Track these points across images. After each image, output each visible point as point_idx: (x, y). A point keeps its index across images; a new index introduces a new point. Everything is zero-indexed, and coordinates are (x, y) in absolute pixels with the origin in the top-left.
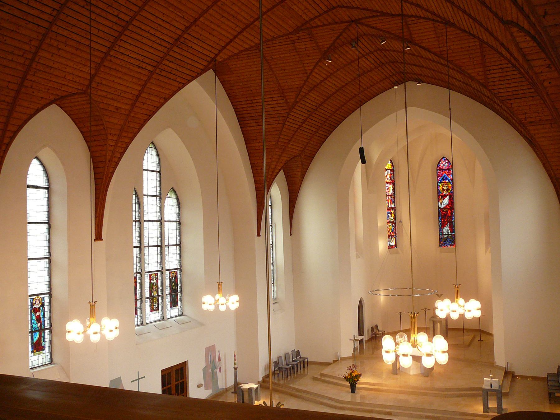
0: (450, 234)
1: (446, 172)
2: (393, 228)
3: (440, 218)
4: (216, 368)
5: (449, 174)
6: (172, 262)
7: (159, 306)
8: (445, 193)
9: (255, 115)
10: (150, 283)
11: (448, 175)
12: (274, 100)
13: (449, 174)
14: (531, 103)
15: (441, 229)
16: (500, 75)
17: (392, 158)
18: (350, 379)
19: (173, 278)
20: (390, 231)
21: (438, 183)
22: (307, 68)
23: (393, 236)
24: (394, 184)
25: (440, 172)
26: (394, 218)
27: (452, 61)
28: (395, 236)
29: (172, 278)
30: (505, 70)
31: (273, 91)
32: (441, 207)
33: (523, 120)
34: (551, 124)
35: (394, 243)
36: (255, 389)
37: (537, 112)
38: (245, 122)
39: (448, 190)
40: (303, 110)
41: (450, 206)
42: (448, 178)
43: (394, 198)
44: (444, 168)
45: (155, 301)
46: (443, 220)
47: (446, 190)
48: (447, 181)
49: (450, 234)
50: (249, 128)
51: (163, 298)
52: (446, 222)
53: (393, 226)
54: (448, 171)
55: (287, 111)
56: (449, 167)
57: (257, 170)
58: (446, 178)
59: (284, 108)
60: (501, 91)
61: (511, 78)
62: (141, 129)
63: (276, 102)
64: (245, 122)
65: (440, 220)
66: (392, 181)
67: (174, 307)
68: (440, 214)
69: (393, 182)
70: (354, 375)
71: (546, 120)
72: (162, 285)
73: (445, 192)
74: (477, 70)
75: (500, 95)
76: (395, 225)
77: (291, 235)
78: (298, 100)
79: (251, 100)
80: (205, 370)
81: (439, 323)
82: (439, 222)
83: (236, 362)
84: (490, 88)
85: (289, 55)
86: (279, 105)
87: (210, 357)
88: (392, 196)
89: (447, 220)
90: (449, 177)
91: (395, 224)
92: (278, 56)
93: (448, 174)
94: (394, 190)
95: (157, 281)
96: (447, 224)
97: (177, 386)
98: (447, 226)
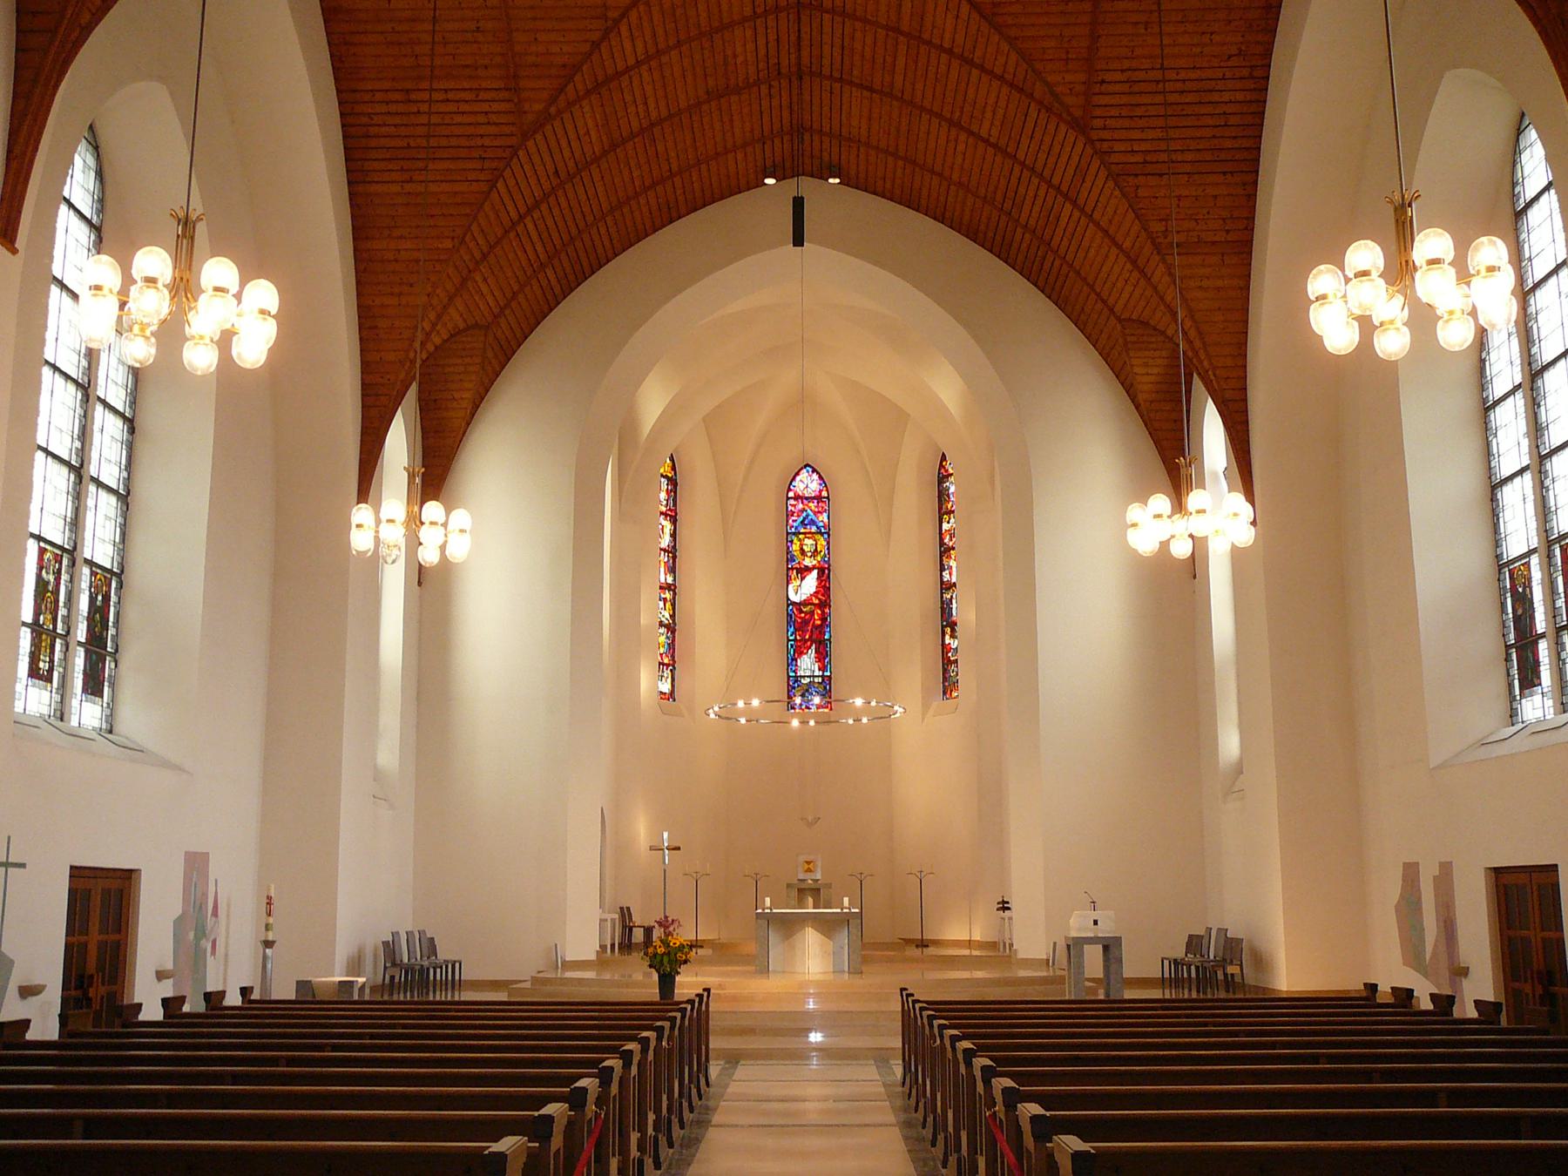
0: (816, 676)
1: (811, 504)
2: (669, 644)
3: (792, 629)
4: (204, 935)
5: (819, 512)
6: (100, 547)
7: (53, 670)
8: (808, 562)
10: (39, 576)
11: (815, 513)
13: (819, 512)
14: (1184, 192)
16: (1125, 100)
19: (100, 598)
20: (662, 652)
21: (788, 533)
24: (674, 521)
25: (795, 503)
26: (670, 616)
28: (671, 668)
29: (97, 595)
30: (1136, 88)
31: (486, 67)
32: (794, 598)
33: (1158, 237)
34: (1223, 255)
37: (1194, 217)
39: (815, 553)
40: (547, 159)
41: (819, 599)
42: (816, 520)
43: (674, 558)
44: (807, 495)
45: (46, 647)
46: (800, 636)
47: (809, 554)
48: (814, 529)
49: (819, 676)
50: (373, 188)
51: (67, 646)
52: (806, 641)
53: (667, 638)
54: (818, 503)
55: (513, 141)
56: (821, 491)
57: (376, 327)
58: (813, 522)
59: (507, 130)
61: (1147, 114)
65: (791, 635)
66: (670, 510)
67: (93, 697)
68: (791, 618)
69: (673, 514)
70: (675, 944)
71: (1214, 243)
72: (69, 601)
73: (807, 560)
76: (674, 637)
77: (420, 583)
78: (553, 110)
80: (179, 923)
82: (789, 640)
83: (271, 920)
84: (1094, 135)
86: (494, 118)
87: (195, 887)
90: (821, 519)
91: (673, 632)
93: (816, 510)
94: (674, 535)
95: (58, 579)
96: (810, 648)
97: (102, 946)
98: (810, 651)
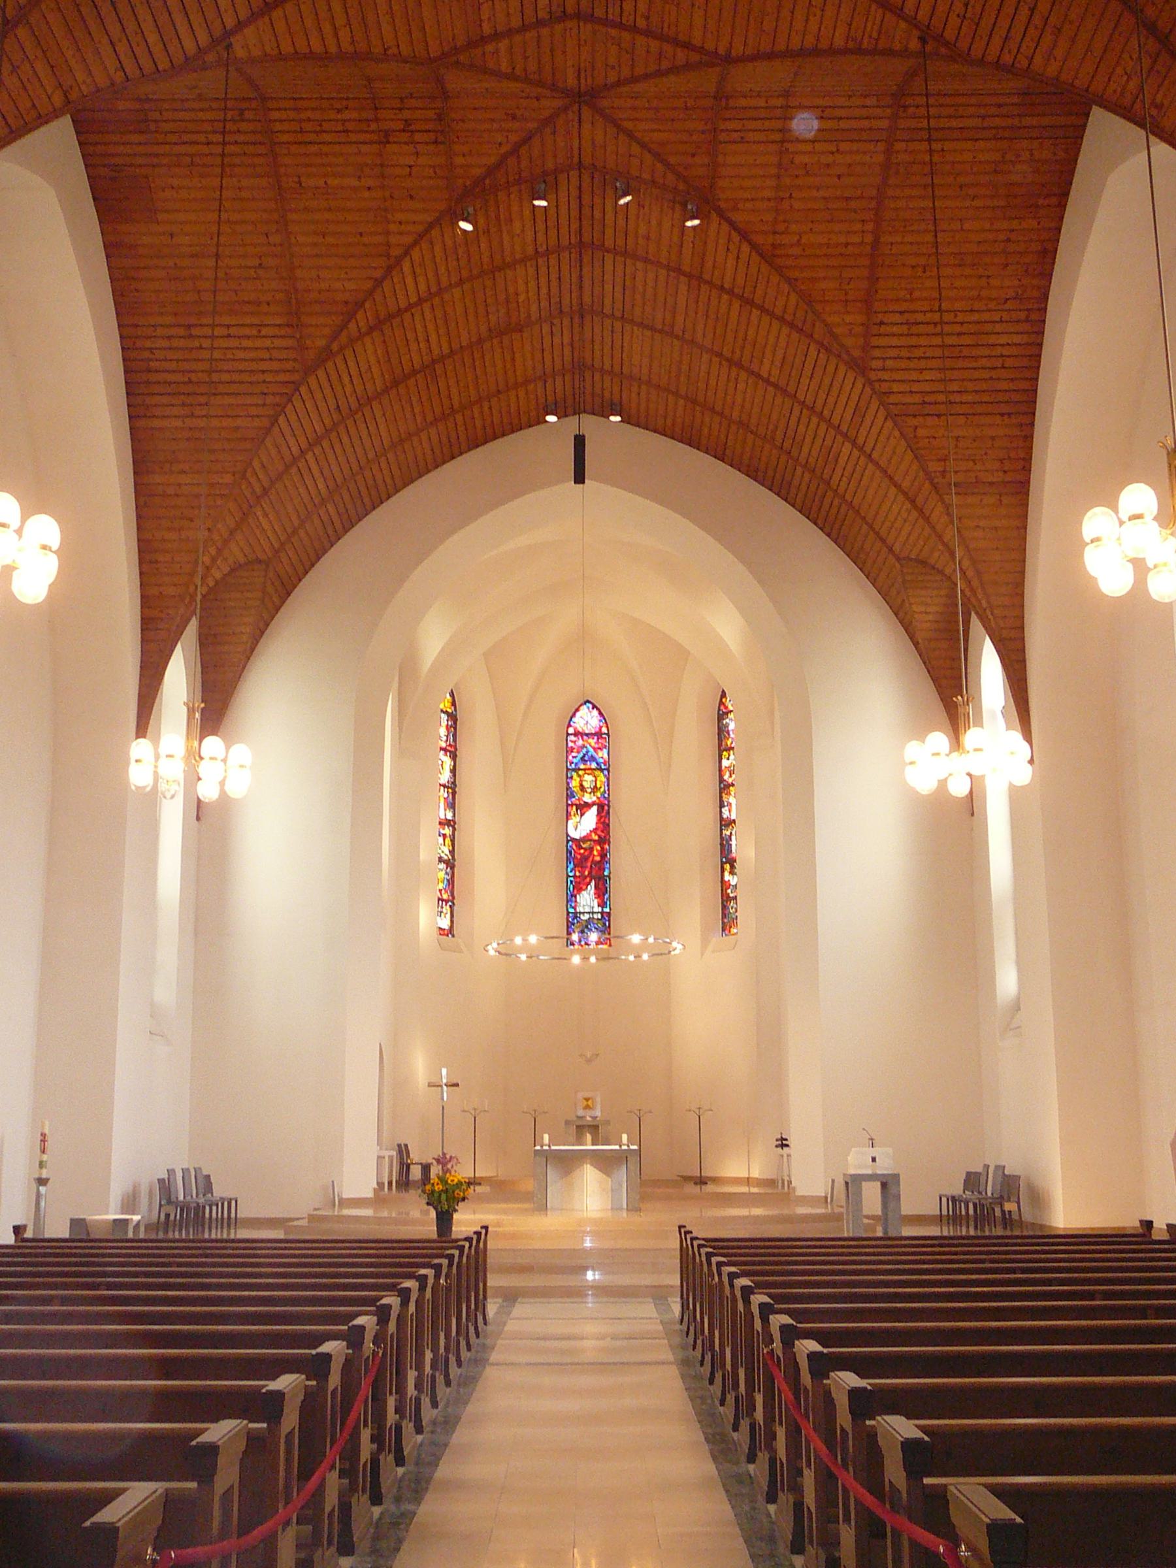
2: (448, 881)
3: (571, 866)
8: (588, 798)
9: (187, 380)
12: (263, 333)
15: (571, 898)
17: (456, 684)
18: (440, 1193)
21: (568, 769)
22: (393, 240)
23: (447, 902)
24: (454, 757)
27: (796, 280)
32: (576, 835)
35: (448, 922)
36: (134, 1223)
38: (150, 400)
39: (595, 789)
42: (596, 757)
43: (454, 793)
47: (589, 790)
50: (156, 423)
53: (447, 873)
55: (296, 377)
56: (601, 727)
60: (896, 387)
62: (20, 136)
63: (268, 343)
64: (150, 400)
66: (450, 745)
69: (453, 750)
74: (848, 319)
75: (893, 399)
77: (198, 818)
78: (335, 347)
79: (189, 326)
81: (590, 1133)
82: (568, 876)
83: (45, 1157)
84: (873, 376)
85: (354, 182)
88: (448, 788)
89: (590, 873)
91: (452, 868)
92: (321, 183)
93: (596, 746)
94: (453, 771)
96: (589, 884)
